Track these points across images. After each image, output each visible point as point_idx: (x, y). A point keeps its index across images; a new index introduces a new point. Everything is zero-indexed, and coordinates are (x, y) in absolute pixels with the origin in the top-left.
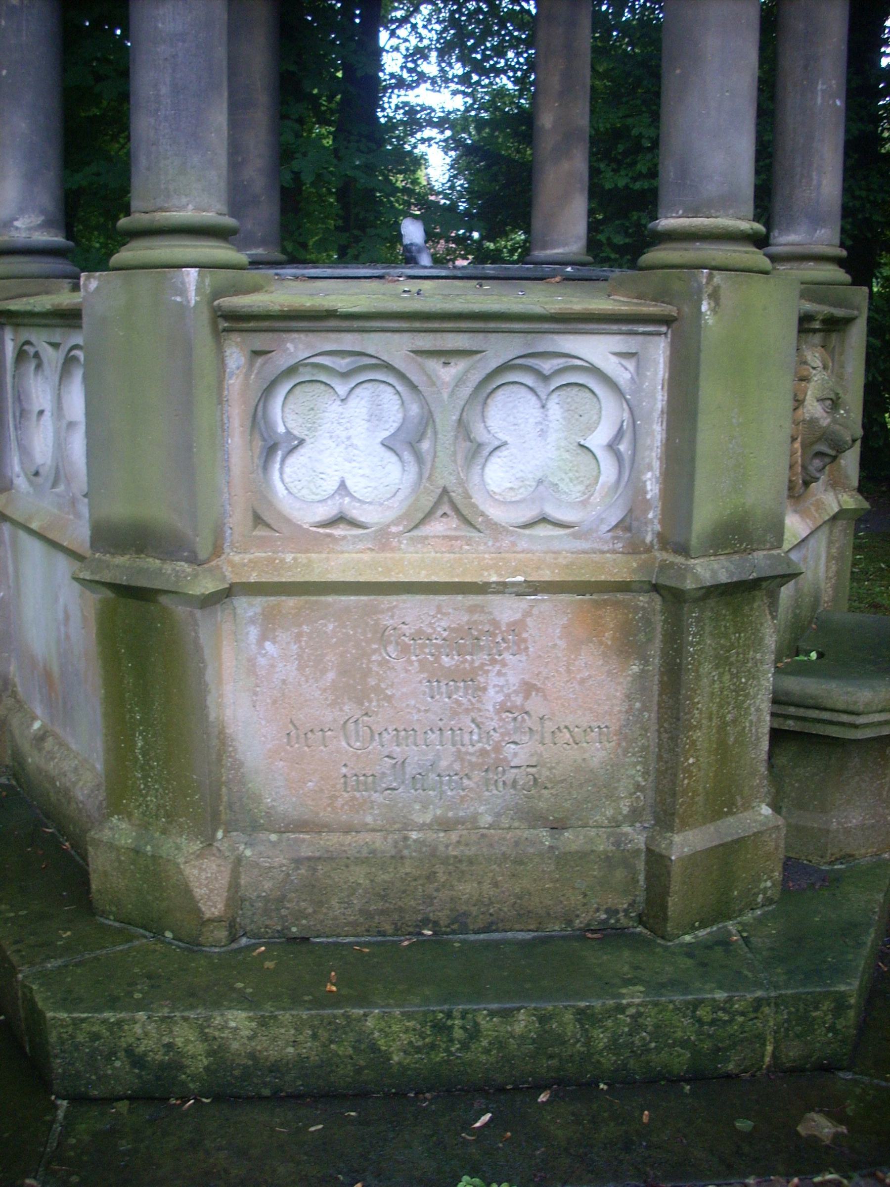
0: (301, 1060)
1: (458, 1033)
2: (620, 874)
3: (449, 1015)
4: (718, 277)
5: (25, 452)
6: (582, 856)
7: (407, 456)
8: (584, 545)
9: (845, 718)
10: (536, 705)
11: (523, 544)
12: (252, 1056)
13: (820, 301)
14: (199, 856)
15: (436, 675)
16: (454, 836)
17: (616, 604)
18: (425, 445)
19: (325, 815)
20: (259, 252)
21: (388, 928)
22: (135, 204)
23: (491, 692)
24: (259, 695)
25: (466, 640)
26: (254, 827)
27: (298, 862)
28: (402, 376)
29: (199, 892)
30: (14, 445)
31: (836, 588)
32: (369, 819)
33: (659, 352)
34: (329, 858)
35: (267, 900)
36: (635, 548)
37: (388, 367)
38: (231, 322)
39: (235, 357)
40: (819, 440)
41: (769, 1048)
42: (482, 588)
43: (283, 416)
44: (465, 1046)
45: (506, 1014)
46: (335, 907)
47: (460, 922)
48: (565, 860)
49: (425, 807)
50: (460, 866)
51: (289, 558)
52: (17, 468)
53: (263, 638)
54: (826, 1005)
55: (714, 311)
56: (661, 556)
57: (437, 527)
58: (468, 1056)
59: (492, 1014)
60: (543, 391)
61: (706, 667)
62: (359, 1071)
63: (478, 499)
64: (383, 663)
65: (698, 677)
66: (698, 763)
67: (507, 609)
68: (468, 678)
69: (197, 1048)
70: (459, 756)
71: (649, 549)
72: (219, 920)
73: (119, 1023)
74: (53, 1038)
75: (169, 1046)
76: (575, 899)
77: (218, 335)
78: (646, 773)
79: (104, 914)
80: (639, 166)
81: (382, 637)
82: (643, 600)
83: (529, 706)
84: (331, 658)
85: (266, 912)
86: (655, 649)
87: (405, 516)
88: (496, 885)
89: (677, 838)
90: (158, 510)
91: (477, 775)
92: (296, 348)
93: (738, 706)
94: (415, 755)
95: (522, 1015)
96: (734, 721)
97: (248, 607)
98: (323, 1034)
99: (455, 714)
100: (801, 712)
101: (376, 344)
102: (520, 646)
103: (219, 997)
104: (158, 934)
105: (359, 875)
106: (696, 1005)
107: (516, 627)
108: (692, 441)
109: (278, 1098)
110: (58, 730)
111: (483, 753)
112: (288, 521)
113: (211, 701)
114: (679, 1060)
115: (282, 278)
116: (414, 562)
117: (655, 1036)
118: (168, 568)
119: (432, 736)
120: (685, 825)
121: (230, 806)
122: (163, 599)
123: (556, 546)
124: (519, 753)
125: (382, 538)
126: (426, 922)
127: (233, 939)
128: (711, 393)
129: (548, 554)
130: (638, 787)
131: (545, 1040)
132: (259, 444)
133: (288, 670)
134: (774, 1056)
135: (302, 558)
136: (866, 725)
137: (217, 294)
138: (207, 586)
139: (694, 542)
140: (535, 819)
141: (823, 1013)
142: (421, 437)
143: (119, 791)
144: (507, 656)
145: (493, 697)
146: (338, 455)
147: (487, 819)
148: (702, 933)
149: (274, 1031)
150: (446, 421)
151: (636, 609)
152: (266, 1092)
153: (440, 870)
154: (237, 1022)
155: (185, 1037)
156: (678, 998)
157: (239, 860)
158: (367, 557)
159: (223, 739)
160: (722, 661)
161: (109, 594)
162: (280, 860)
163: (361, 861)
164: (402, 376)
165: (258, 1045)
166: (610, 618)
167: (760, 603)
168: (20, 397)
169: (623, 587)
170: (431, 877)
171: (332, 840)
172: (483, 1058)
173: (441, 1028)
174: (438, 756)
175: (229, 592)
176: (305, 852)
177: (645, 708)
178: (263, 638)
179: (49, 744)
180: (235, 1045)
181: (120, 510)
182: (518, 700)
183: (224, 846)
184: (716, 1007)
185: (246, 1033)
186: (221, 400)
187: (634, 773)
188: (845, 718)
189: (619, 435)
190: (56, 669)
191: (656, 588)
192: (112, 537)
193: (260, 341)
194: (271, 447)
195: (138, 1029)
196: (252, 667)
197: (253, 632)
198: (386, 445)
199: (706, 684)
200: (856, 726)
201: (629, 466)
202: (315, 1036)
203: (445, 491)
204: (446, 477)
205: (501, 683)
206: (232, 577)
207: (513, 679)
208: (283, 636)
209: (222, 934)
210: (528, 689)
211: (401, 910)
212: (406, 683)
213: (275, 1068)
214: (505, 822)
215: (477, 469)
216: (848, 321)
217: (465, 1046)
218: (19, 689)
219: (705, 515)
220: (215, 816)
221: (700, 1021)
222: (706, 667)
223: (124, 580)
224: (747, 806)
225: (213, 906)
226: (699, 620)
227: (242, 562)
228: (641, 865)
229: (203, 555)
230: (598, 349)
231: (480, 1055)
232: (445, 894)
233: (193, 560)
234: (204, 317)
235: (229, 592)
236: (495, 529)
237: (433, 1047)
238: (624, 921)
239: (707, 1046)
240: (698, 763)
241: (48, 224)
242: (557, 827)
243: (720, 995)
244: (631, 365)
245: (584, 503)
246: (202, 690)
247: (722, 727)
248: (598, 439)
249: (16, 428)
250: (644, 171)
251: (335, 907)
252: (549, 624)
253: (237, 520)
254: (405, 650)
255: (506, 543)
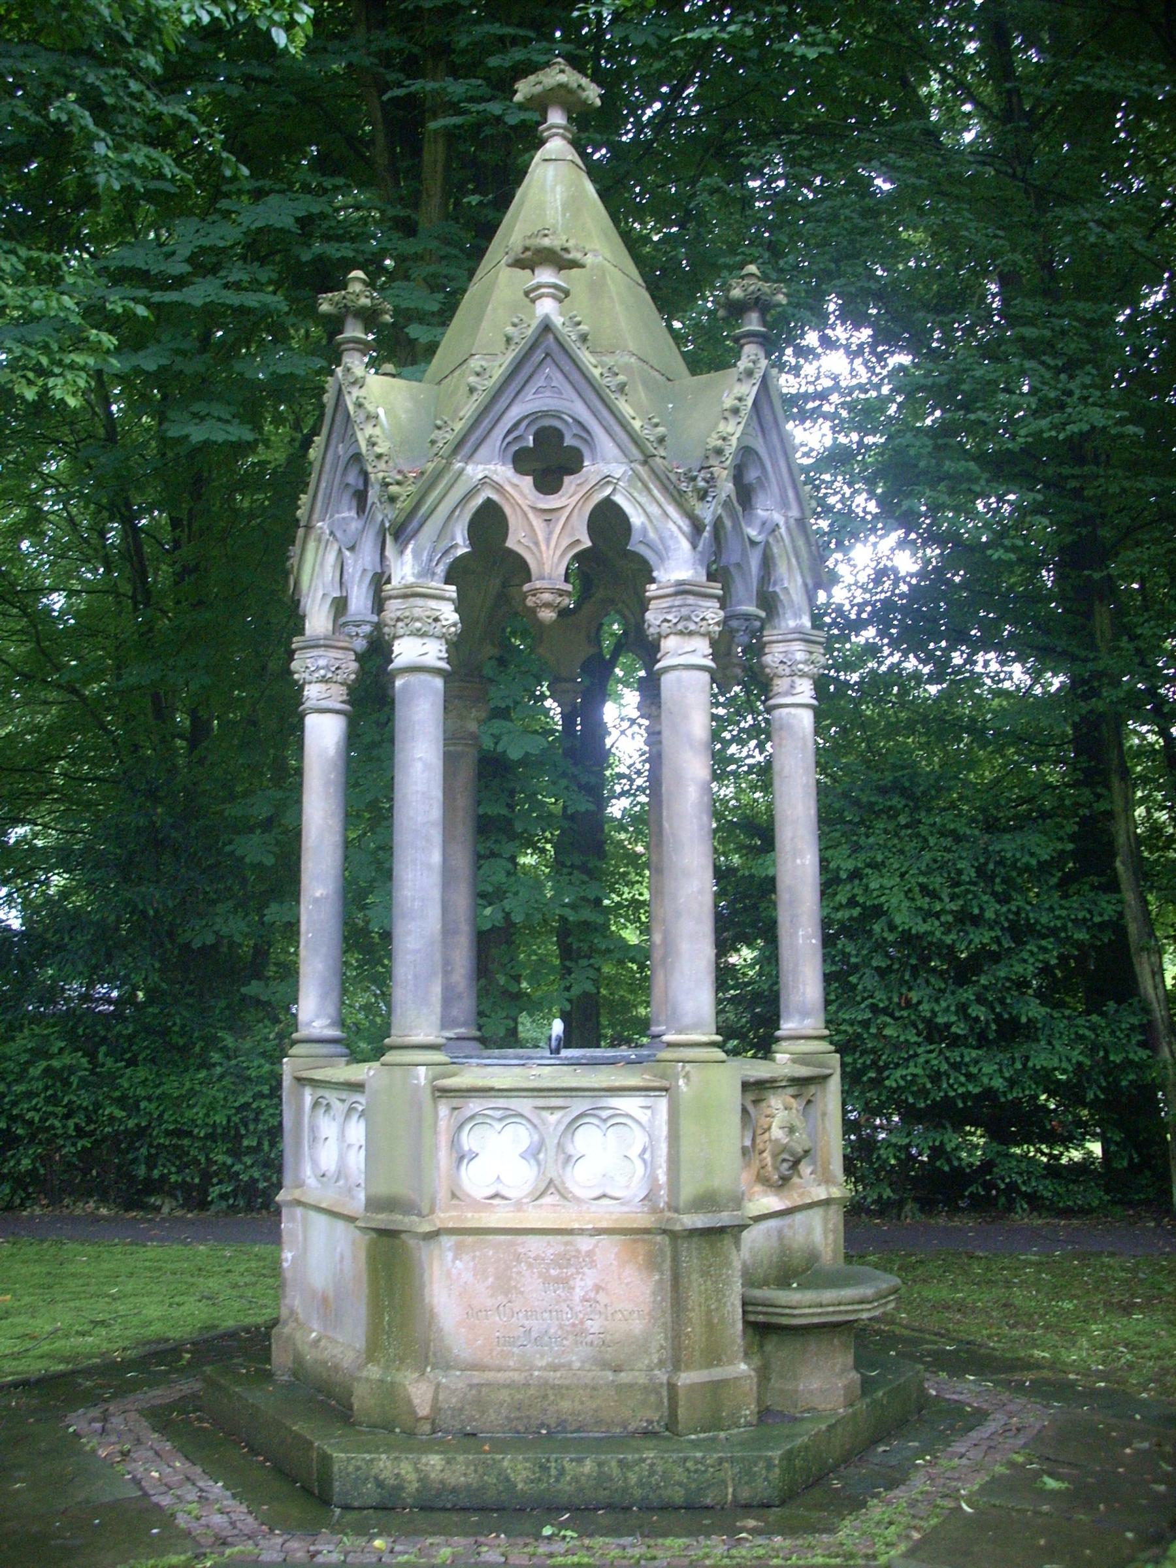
0: (468, 1486)
1: (553, 1472)
2: (652, 1398)
3: (548, 1460)
4: (688, 1067)
5: (315, 1163)
6: (631, 1386)
7: (532, 1161)
8: (626, 1209)
9: (787, 1311)
10: (602, 1298)
11: (593, 1209)
12: (442, 1482)
13: (807, 1064)
14: (417, 1381)
15: (547, 1280)
16: (558, 1374)
17: (644, 1241)
18: (541, 1156)
19: (487, 1360)
20: (461, 1031)
21: (521, 1428)
22: (393, 1032)
23: (577, 1290)
24: (451, 1289)
25: (562, 1260)
26: (448, 1367)
27: (471, 1386)
28: (529, 1121)
29: (416, 1401)
30: (307, 1159)
31: (834, 1251)
32: (511, 1363)
33: (662, 1104)
34: (488, 1385)
35: (453, 1409)
36: (654, 1210)
37: (521, 1116)
38: (443, 1093)
39: (443, 1110)
40: (783, 1151)
41: (730, 1490)
42: (570, 1232)
43: (469, 1140)
44: (557, 1481)
45: (580, 1461)
46: (492, 1415)
47: (562, 1423)
48: (620, 1388)
49: (542, 1356)
50: (560, 1390)
51: (469, 1215)
52: (309, 1173)
53: (455, 1258)
54: (761, 1464)
55: (687, 1084)
56: (668, 1214)
57: (547, 1200)
58: (559, 1486)
59: (572, 1460)
60: (604, 1127)
61: (695, 1276)
62: (500, 1493)
63: (569, 1184)
64: (519, 1273)
65: (690, 1281)
66: (694, 1330)
67: (585, 1244)
68: (564, 1281)
69: (413, 1476)
70: (561, 1327)
71: (662, 1211)
72: (426, 1418)
73: (372, 1460)
74: (336, 1468)
75: (398, 1475)
76: (627, 1413)
77: (435, 1099)
78: (666, 1339)
79: (360, 1424)
80: (838, 898)
81: (518, 1258)
82: (659, 1238)
83: (599, 1298)
84: (491, 1270)
85: (453, 1417)
86: (667, 1264)
87: (531, 1193)
88: (582, 1403)
89: (683, 1375)
90: (401, 1189)
91: (571, 1337)
92: (474, 1106)
93: (719, 1301)
94: (535, 1325)
95: (588, 1462)
96: (717, 1309)
97: (447, 1241)
98: (480, 1470)
99: (558, 1303)
100: (765, 1309)
101: (515, 1104)
102: (592, 1264)
103: (428, 1447)
104: (392, 1431)
105: (504, 1395)
106: (685, 1460)
107: (590, 1253)
108: (678, 1152)
109: (455, 1509)
110: (330, 1334)
111: (574, 1325)
112: (469, 1196)
113: (426, 1290)
114: (678, 1495)
115: (470, 1065)
116: (534, 1218)
117: (663, 1478)
118: (407, 1219)
119: (546, 1315)
120: (688, 1368)
121: (435, 1354)
122: (403, 1236)
123: (611, 1209)
124: (594, 1326)
125: (519, 1206)
126: (542, 1425)
127: (434, 1432)
128: (687, 1127)
129: (606, 1214)
130: (662, 1347)
131: (602, 1479)
132: (454, 1155)
133: (467, 1276)
134: (734, 1495)
135: (476, 1215)
136: (801, 1315)
137: (435, 1079)
138: (426, 1228)
139: (682, 1205)
140: (604, 1365)
141: (759, 1468)
142: (539, 1152)
143: (373, 1351)
144: (585, 1270)
145: (578, 1293)
146: (494, 1162)
147: (577, 1365)
148: (702, 1435)
149: (454, 1467)
150: (552, 1142)
151: (655, 1244)
152: (449, 1506)
153: (550, 1392)
154: (434, 1461)
155: (406, 1469)
156: (675, 1456)
157: (438, 1385)
158: (511, 1215)
159: (432, 1315)
160: (705, 1273)
161: (374, 1235)
162: (460, 1385)
163: (507, 1386)
164: (529, 1121)
165: (446, 1475)
166: (641, 1249)
167: (728, 1241)
168: (313, 1129)
169: (647, 1231)
170: (545, 1397)
171: (490, 1376)
172: (568, 1488)
173: (544, 1468)
174: (549, 1326)
175: (436, 1234)
176: (475, 1381)
177: (663, 1300)
178: (455, 1258)
179: (323, 1343)
180: (433, 1476)
181: (382, 1189)
182: (592, 1295)
183: (431, 1376)
184: (697, 1462)
185: (439, 1468)
186: (436, 1133)
187: (659, 1338)
188: (787, 1311)
189: (644, 1150)
190: (331, 1295)
191: (665, 1232)
192: (375, 1204)
193: (456, 1102)
194: (461, 1157)
195: (381, 1464)
196: (449, 1274)
197: (450, 1255)
198: (522, 1156)
199: (696, 1288)
200: (794, 1316)
201: (650, 1166)
202: (476, 1471)
203: (551, 1181)
204: (552, 1174)
205: (582, 1285)
206: (439, 1225)
207: (590, 1283)
208: (466, 1257)
209: (427, 1428)
210: (598, 1288)
211: (528, 1417)
212: (531, 1284)
213: (454, 1490)
214: (587, 1366)
215: (569, 1169)
216: (826, 1077)
217: (557, 1481)
218: (301, 1316)
219: (687, 1192)
220: (426, 1361)
221: (688, 1470)
222: (695, 1276)
223: (383, 1226)
224: (731, 1362)
225: (424, 1410)
226: (688, 1249)
227: (444, 1217)
228: (665, 1393)
229: (425, 1212)
230: (629, 1104)
231: (566, 1486)
232: (552, 1408)
233: (420, 1215)
234: (428, 1091)
235: (436, 1234)
236: (578, 1200)
237: (540, 1480)
238: (657, 1428)
239: (693, 1486)
240: (694, 1330)
241: (333, 1024)
242: (617, 1370)
243: (699, 1455)
244: (649, 1112)
245: (628, 1187)
246: (422, 1286)
247: (709, 1312)
248: (634, 1153)
249: (310, 1148)
250: (844, 901)
251: (492, 1415)
252: (608, 1250)
253: (443, 1195)
254: (530, 1266)
255: (584, 1207)
